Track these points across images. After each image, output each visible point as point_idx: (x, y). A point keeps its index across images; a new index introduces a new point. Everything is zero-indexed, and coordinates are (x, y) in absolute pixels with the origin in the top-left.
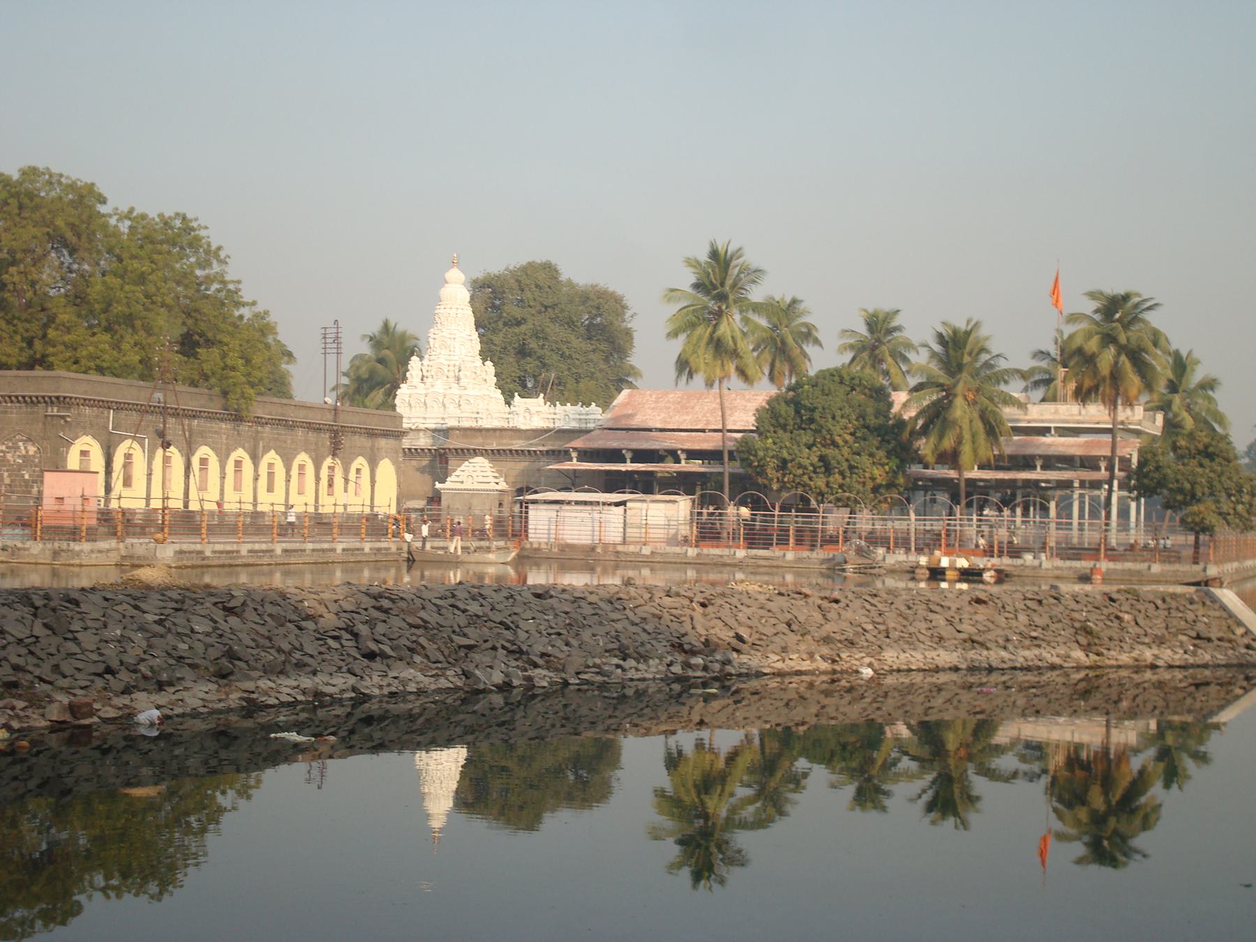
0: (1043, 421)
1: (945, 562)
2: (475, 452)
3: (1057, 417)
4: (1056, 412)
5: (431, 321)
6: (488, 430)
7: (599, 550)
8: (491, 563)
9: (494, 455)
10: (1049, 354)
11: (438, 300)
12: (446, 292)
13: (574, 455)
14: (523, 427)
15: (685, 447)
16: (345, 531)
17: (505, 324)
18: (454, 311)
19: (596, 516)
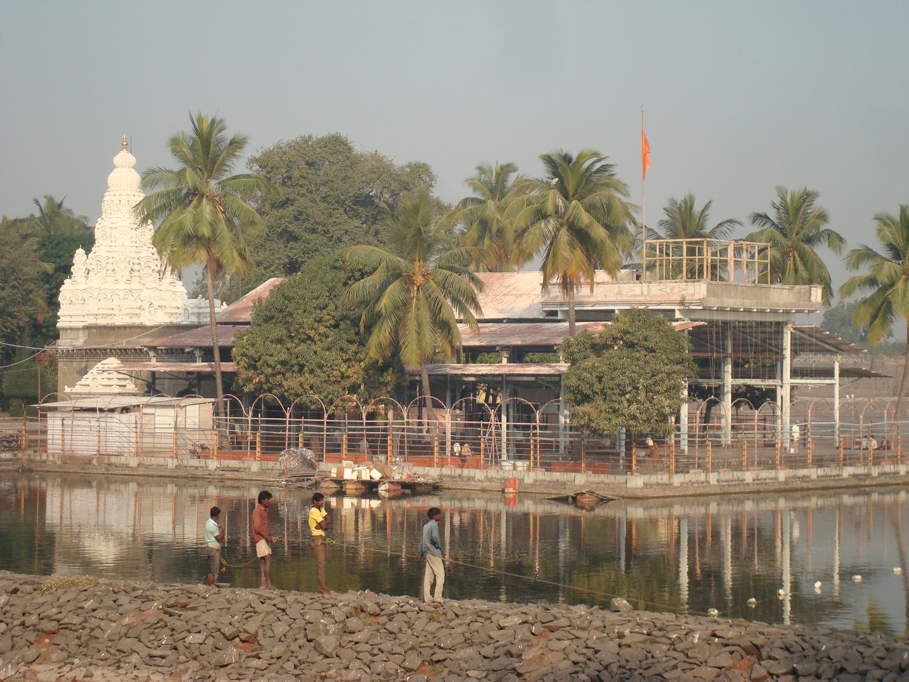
0: (606, 303)
1: (348, 475)
2: (105, 353)
3: (619, 298)
4: (620, 293)
5: (99, 214)
6: (119, 328)
7: (95, 462)
8: (635, 499)
9: (122, 353)
10: (766, 217)
11: (105, 187)
12: (113, 178)
13: (197, 353)
14: (148, 324)
15: (202, 344)
16: (848, 461)
17: (273, 206)
18: (117, 198)
19: (94, 423)
